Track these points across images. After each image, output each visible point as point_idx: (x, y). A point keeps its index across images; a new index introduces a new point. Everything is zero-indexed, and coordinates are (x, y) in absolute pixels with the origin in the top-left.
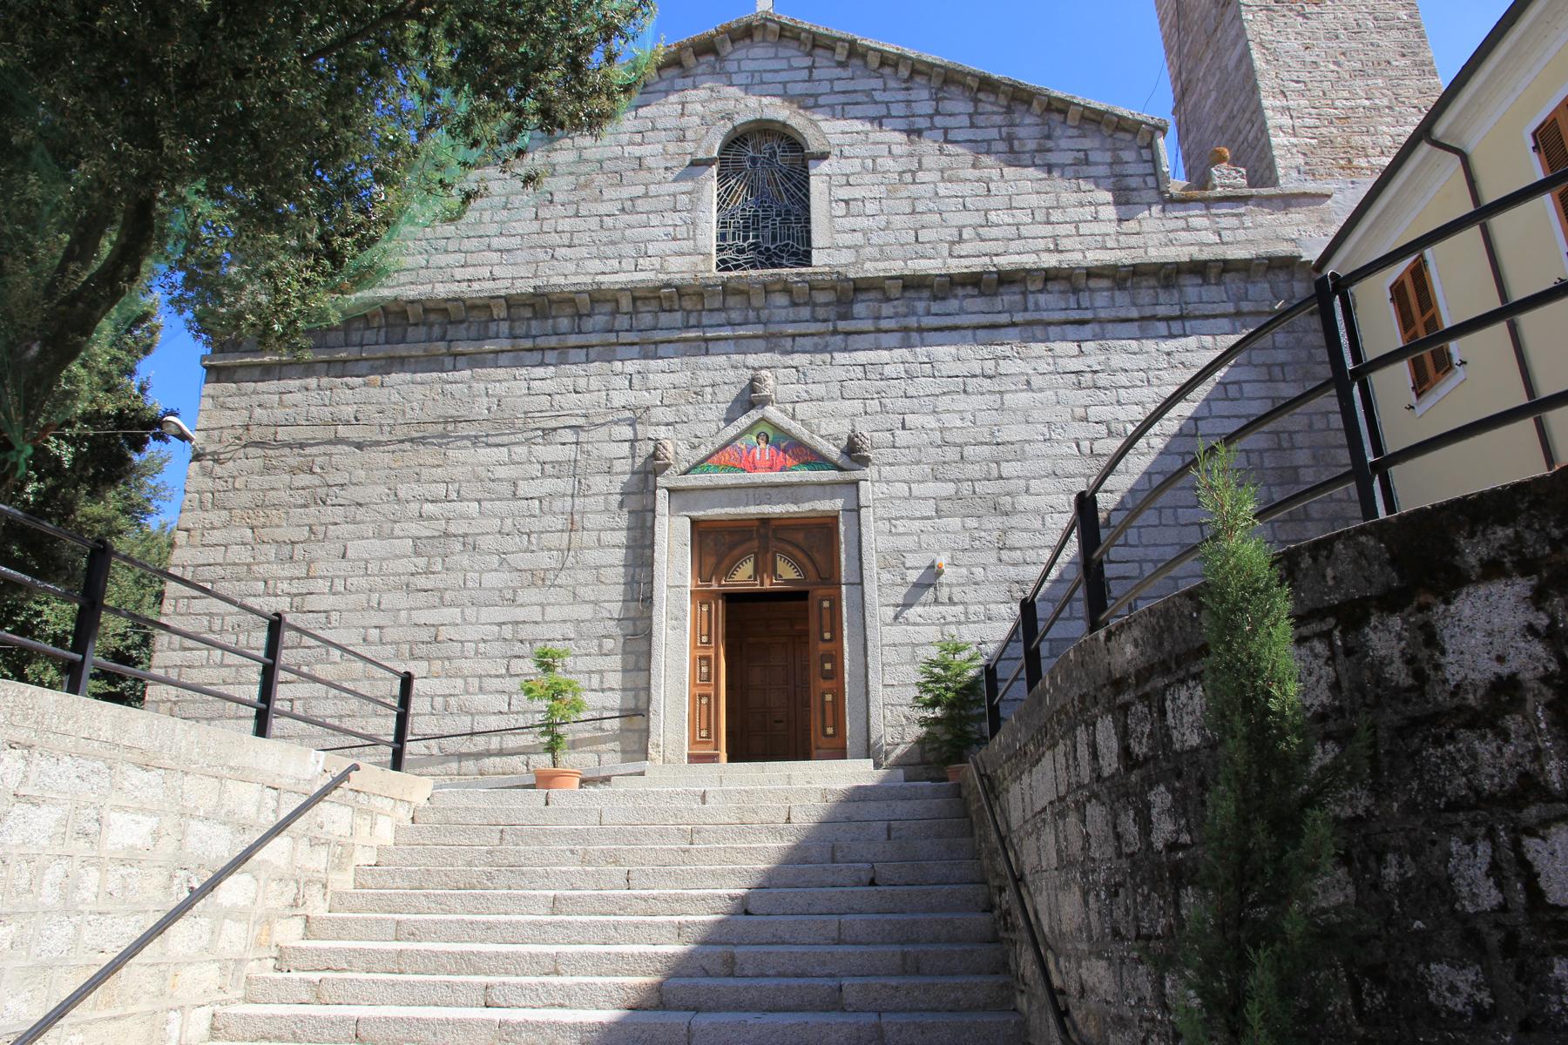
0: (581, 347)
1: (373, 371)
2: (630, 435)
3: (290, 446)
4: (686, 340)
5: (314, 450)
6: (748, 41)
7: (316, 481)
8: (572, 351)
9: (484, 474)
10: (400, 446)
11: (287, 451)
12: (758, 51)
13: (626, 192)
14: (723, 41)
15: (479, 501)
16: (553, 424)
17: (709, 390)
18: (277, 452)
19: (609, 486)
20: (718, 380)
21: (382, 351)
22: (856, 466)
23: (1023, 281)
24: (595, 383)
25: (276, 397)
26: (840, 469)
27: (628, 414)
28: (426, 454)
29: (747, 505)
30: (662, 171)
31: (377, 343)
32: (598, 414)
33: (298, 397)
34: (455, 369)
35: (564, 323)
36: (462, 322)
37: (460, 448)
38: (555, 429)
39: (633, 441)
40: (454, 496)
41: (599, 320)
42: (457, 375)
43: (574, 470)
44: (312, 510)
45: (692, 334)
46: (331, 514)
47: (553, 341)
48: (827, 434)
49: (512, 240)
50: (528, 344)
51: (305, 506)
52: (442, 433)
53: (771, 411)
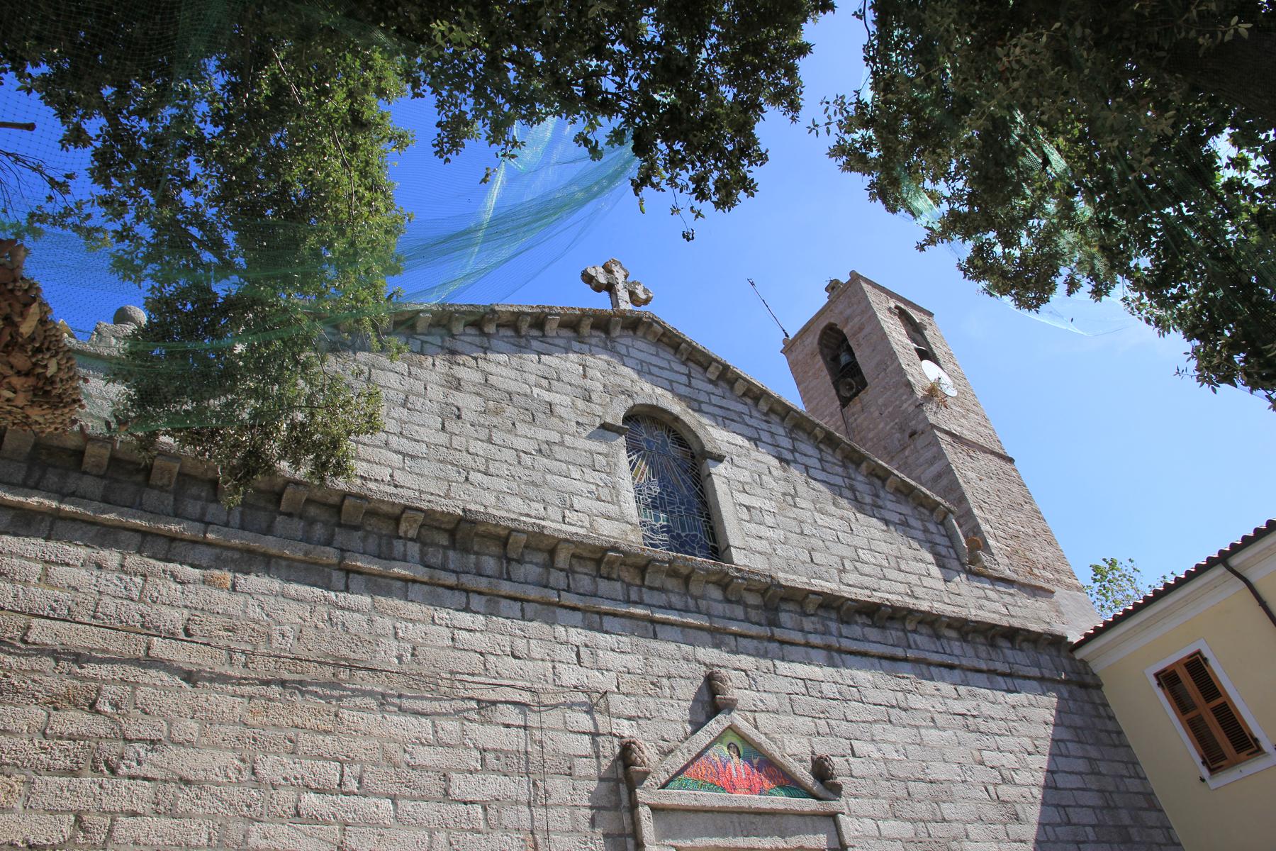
1: (219, 563)
2: (589, 726)
3: (56, 655)
5: (103, 671)
7: (100, 727)
8: (504, 602)
9: (399, 756)
10: (262, 689)
11: (48, 663)
12: (640, 344)
13: (542, 435)
14: (617, 323)
15: (394, 799)
16: (491, 695)
17: (665, 681)
18: (25, 663)
19: (574, 794)
20: (673, 671)
21: (238, 540)
22: (831, 795)
23: (904, 619)
24: (537, 650)
25: (37, 568)
26: (819, 799)
27: (582, 697)
28: (306, 709)
29: (735, 836)
31: (227, 525)
32: (545, 691)
33: (82, 576)
34: (347, 589)
35: (490, 564)
36: (356, 528)
37: (360, 709)
38: (494, 703)
39: (595, 735)
40: (353, 785)
41: (531, 570)
42: (353, 599)
43: (526, 765)
44: (87, 781)
46: (122, 793)
47: (483, 584)
48: (794, 750)
50: (451, 579)
51: (71, 773)
52: (333, 679)
53: (737, 718)
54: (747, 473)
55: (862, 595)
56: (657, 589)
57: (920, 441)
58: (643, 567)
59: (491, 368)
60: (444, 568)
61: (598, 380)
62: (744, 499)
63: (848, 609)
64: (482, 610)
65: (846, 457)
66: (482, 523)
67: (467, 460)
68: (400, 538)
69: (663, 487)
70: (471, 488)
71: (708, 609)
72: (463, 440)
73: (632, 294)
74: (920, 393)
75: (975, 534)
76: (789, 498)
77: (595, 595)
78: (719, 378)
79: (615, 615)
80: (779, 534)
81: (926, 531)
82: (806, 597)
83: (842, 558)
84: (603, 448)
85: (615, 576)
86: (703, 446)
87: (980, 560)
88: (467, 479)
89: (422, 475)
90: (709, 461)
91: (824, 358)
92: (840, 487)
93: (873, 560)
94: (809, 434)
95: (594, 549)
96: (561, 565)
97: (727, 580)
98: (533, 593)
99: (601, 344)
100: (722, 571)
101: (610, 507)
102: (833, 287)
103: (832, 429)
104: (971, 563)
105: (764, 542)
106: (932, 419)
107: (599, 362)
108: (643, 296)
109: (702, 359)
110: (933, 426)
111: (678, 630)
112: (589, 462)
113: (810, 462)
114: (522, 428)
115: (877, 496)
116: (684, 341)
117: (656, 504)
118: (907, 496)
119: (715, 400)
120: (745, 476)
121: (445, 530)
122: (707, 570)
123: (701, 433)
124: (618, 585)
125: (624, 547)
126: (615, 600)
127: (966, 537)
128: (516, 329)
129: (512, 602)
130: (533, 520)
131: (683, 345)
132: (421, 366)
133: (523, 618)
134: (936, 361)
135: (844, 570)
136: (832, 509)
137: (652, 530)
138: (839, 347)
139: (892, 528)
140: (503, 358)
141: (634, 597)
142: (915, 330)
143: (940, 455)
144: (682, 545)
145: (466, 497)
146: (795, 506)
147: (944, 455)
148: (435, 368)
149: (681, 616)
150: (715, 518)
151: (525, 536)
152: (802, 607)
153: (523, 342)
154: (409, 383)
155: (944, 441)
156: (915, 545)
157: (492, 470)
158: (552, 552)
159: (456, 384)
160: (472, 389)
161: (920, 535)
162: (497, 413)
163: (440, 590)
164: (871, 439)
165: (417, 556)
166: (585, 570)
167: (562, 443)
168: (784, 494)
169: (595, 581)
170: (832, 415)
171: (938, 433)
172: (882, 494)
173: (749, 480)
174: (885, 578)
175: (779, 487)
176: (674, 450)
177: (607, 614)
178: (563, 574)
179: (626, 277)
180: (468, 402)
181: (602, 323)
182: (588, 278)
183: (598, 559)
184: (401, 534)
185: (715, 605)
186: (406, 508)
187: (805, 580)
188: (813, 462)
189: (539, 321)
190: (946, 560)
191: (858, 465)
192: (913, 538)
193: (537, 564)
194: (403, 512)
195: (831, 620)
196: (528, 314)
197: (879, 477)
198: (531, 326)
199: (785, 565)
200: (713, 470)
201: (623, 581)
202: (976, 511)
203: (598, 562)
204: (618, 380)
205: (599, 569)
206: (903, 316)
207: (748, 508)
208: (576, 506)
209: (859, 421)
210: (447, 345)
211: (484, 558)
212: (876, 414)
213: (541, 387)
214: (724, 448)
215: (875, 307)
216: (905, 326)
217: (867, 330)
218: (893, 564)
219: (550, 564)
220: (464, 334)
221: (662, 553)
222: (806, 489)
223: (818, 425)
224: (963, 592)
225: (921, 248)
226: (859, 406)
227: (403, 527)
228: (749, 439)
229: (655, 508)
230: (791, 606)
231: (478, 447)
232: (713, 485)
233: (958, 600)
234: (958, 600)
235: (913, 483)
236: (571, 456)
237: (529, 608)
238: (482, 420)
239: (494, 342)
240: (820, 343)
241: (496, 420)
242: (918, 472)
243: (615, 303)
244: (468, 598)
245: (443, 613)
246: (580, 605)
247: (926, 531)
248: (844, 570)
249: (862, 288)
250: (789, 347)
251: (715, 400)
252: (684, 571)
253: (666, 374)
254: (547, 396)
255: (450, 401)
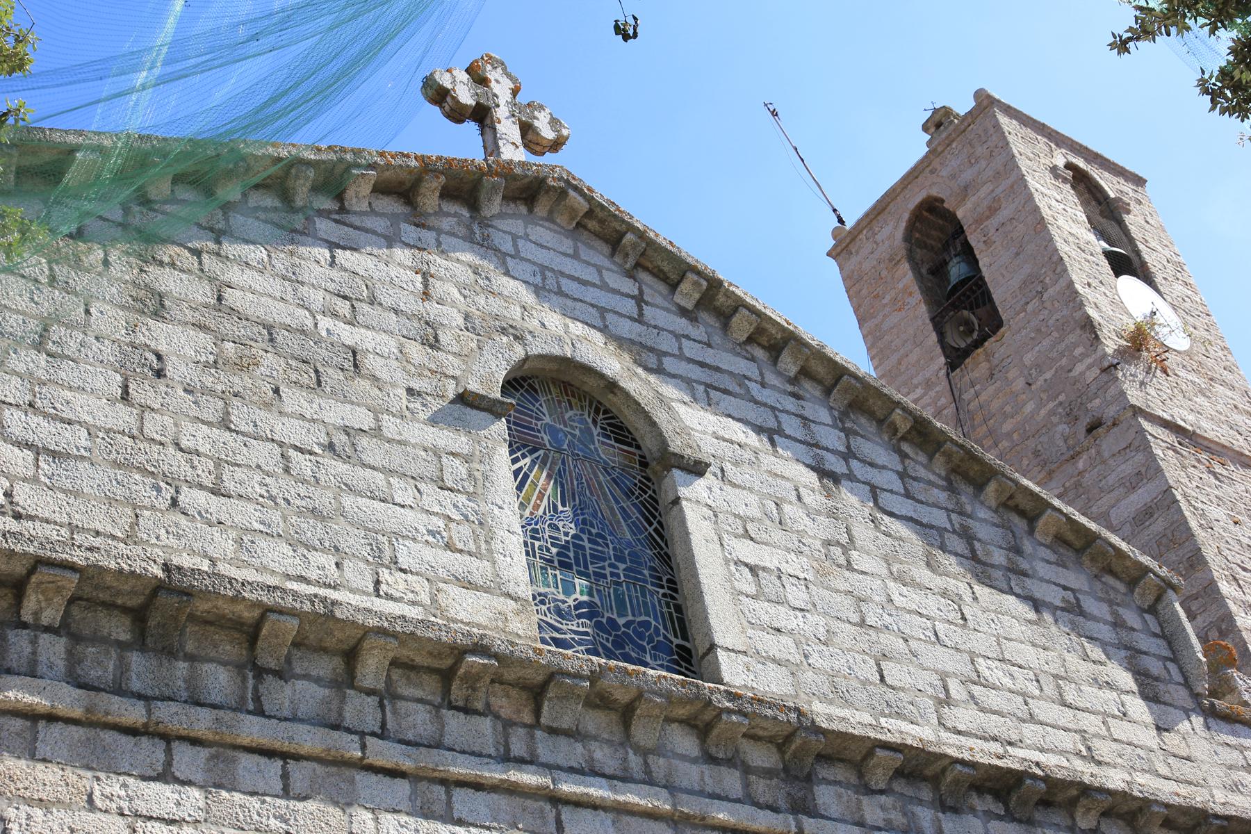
0: (269, 753)
4: (512, 790)
6: (523, 209)
8: (246, 760)
12: (541, 233)
13: (337, 413)
14: (494, 188)
23: (1072, 804)
30: (402, 392)
35: (219, 680)
41: (305, 694)
45: (528, 778)
47: (202, 722)
49: (67, 433)
50: (134, 713)
54: (752, 499)
55: (984, 753)
56: (567, 733)
57: (1109, 442)
58: (538, 688)
59: (234, 274)
60: (119, 690)
61: (453, 304)
62: (746, 551)
63: (956, 782)
64: (198, 777)
65: (954, 470)
66: (206, 594)
67: (174, 462)
68: (25, 626)
69: (583, 525)
70: (183, 521)
71: (669, 774)
72: (169, 421)
73: (527, 129)
74: (1110, 345)
75: (1223, 634)
76: (837, 551)
77: (438, 745)
78: (698, 304)
79: (477, 786)
80: (815, 624)
81: (1118, 624)
82: (870, 754)
83: (943, 677)
84: (461, 442)
85: (479, 706)
86: (664, 443)
87: (1233, 689)
88: (174, 503)
89: (77, 494)
90: (676, 473)
91: (916, 268)
92: (941, 531)
93: (1007, 681)
94: (880, 422)
95: (439, 649)
96: (368, 683)
97: (708, 715)
98: (309, 739)
99: (462, 231)
100: (698, 697)
101: (474, 564)
102: (939, 122)
103: (927, 414)
104: (1213, 693)
105: (785, 640)
106: (1135, 396)
107: (456, 266)
108: (548, 134)
109: (666, 267)
110: (1137, 411)
111: (608, 818)
112: (432, 470)
113: (880, 478)
114: (293, 399)
115: (1018, 551)
116: (631, 228)
117: (567, 560)
118: (1079, 551)
119: (690, 349)
120: (746, 504)
121: (125, 610)
122: (668, 696)
123: (660, 417)
124: (486, 724)
125: (499, 645)
126: (480, 755)
127: (1203, 639)
128: (286, 197)
129: (263, 760)
130: (311, 590)
131: (629, 237)
132: (77, 264)
133: (286, 793)
134: (1148, 279)
135: (946, 701)
136: (922, 574)
137: (559, 612)
138: (946, 247)
139: (1048, 617)
140: (257, 254)
141: (518, 749)
142: (1106, 213)
143: (1152, 469)
144: (618, 643)
145: (172, 541)
146: (849, 567)
147: (1159, 470)
148: (109, 274)
149: (613, 789)
150: (686, 588)
151: (293, 623)
152: (861, 775)
153: (299, 221)
154: (49, 299)
155: (1160, 441)
156: (1096, 652)
157: (229, 485)
158: (351, 656)
159: (156, 306)
160: (189, 316)
161: (1106, 632)
162: (243, 365)
163: (108, 736)
164: (1009, 435)
165: (61, 664)
166: (419, 693)
167: (377, 432)
168: (828, 543)
169: (439, 717)
170: (928, 384)
171: (1146, 425)
172: (1027, 546)
173: (756, 513)
174: (1032, 719)
175: (818, 529)
176: (607, 451)
177: (462, 784)
178: (372, 701)
179: (515, 92)
180: (178, 342)
181: (465, 187)
182: (439, 96)
183: (448, 670)
184: (27, 617)
185: (683, 767)
186: (39, 562)
187: (867, 719)
188: (887, 479)
189: (333, 179)
190: (1161, 687)
191: (979, 487)
192: (1091, 639)
193: (318, 681)
194: (32, 571)
195: (920, 802)
196: (309, 163)
197: (1022, 513)
198: (316, 189)
199: (826, 688)
200: (683, 492)
201: (497, 717)
202: (1225, 588)
203: (447, 676)
204: (495, 305)
205: (446, 691)
206: (1082, 183)
207: (753, 569)
208: (404, 562)
209: (983, 397)
210: (136, 220)
211: (207, 667)
212: (1020, 383)
213: (335, 315)
214: (707, 447)
215: (1023, 164)
216: (1085, 204)
217: (1005, 213)
218: (1049, 689)
219: (347, 680)
220: (173, 200)
221: (578, 659)
222: (871, 533)
223: (898, 404)
224: (1195, 753)
225: (1121, 46)
226: (984, 366)
227: (31, 603)
228: (759, 430)
229: (565, 566)
230: (838, 772)
231: (201, 437)
232: (683, 521)
233: (1187, 769)
234: (1187, 769)
235: (1093, 526)
236: (396, 458)
237: (300, 773)
238: (209, 381)
239: (237, 220)
240: (908, 237)
241: (239, 382)
242: (1106, 501)
243: (492, 147)
244: (168, 752)
245: (113, 786)
246: (407, 765)
247: (1118, 624)
248: (946, 701)
249: (997, 126)
250: (845, 245)
251: (690, 349)
252: (622, 696)
253: (592, 295)
254: (349, 336)
255: (140, 339)
